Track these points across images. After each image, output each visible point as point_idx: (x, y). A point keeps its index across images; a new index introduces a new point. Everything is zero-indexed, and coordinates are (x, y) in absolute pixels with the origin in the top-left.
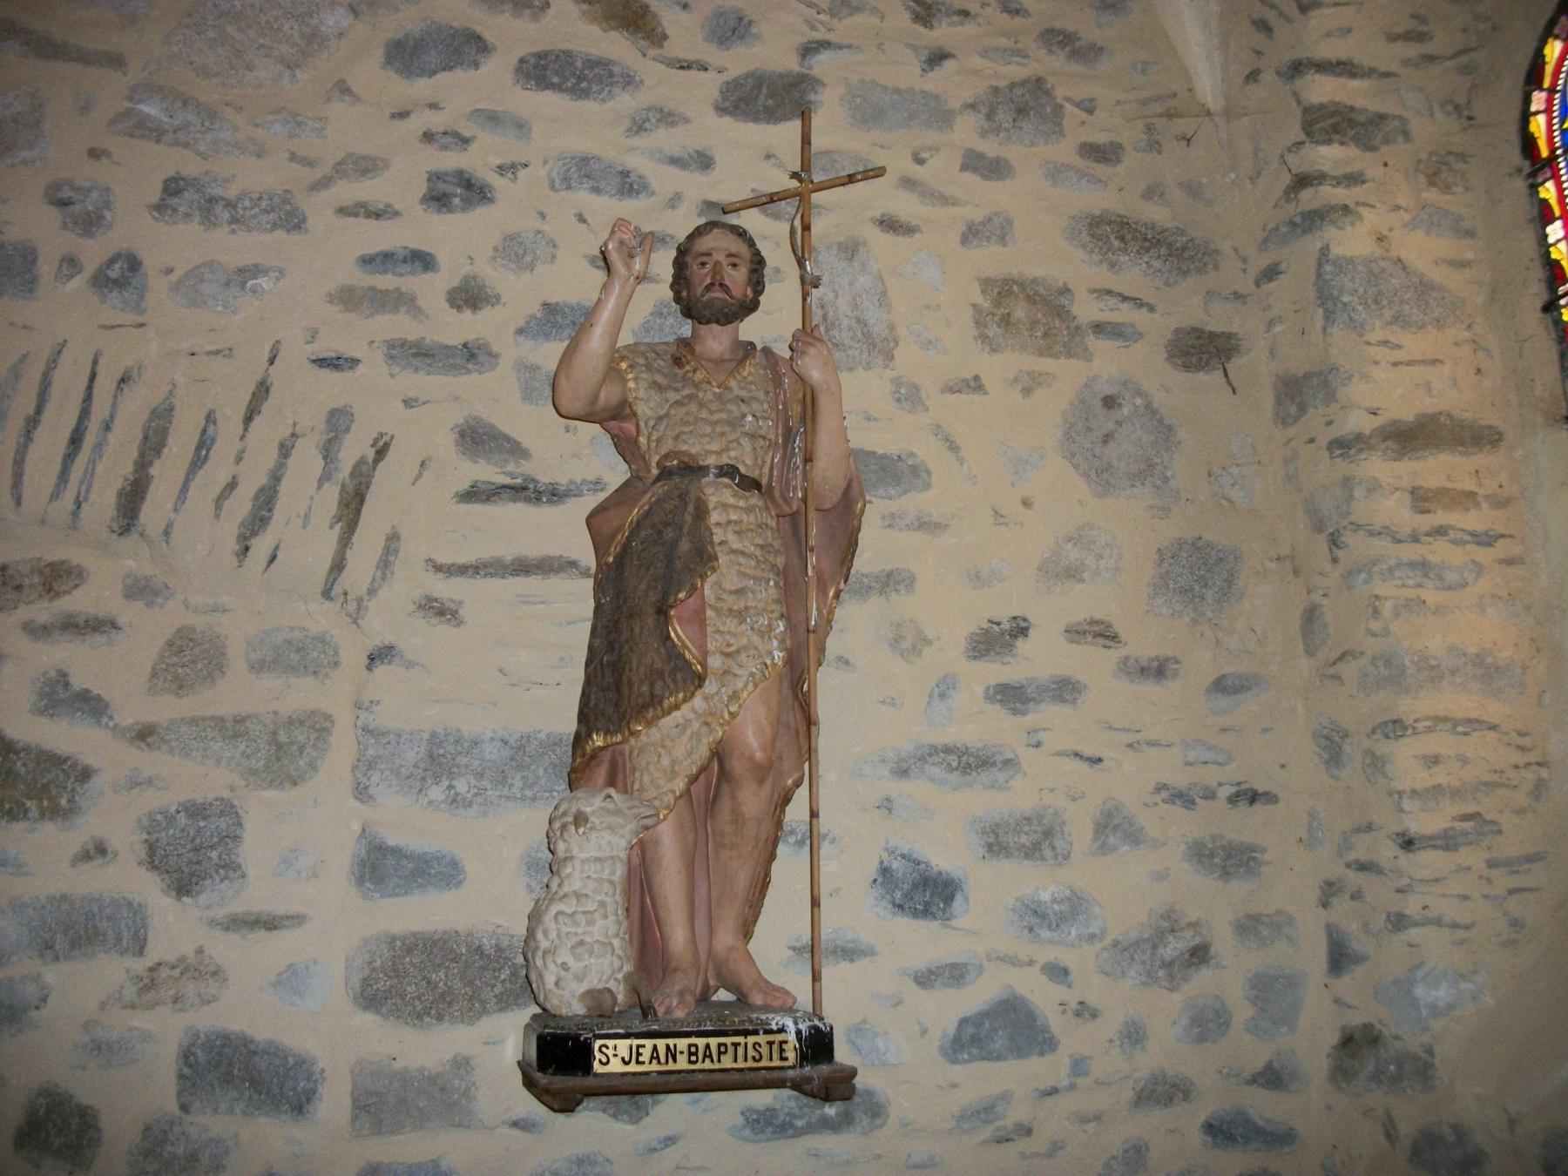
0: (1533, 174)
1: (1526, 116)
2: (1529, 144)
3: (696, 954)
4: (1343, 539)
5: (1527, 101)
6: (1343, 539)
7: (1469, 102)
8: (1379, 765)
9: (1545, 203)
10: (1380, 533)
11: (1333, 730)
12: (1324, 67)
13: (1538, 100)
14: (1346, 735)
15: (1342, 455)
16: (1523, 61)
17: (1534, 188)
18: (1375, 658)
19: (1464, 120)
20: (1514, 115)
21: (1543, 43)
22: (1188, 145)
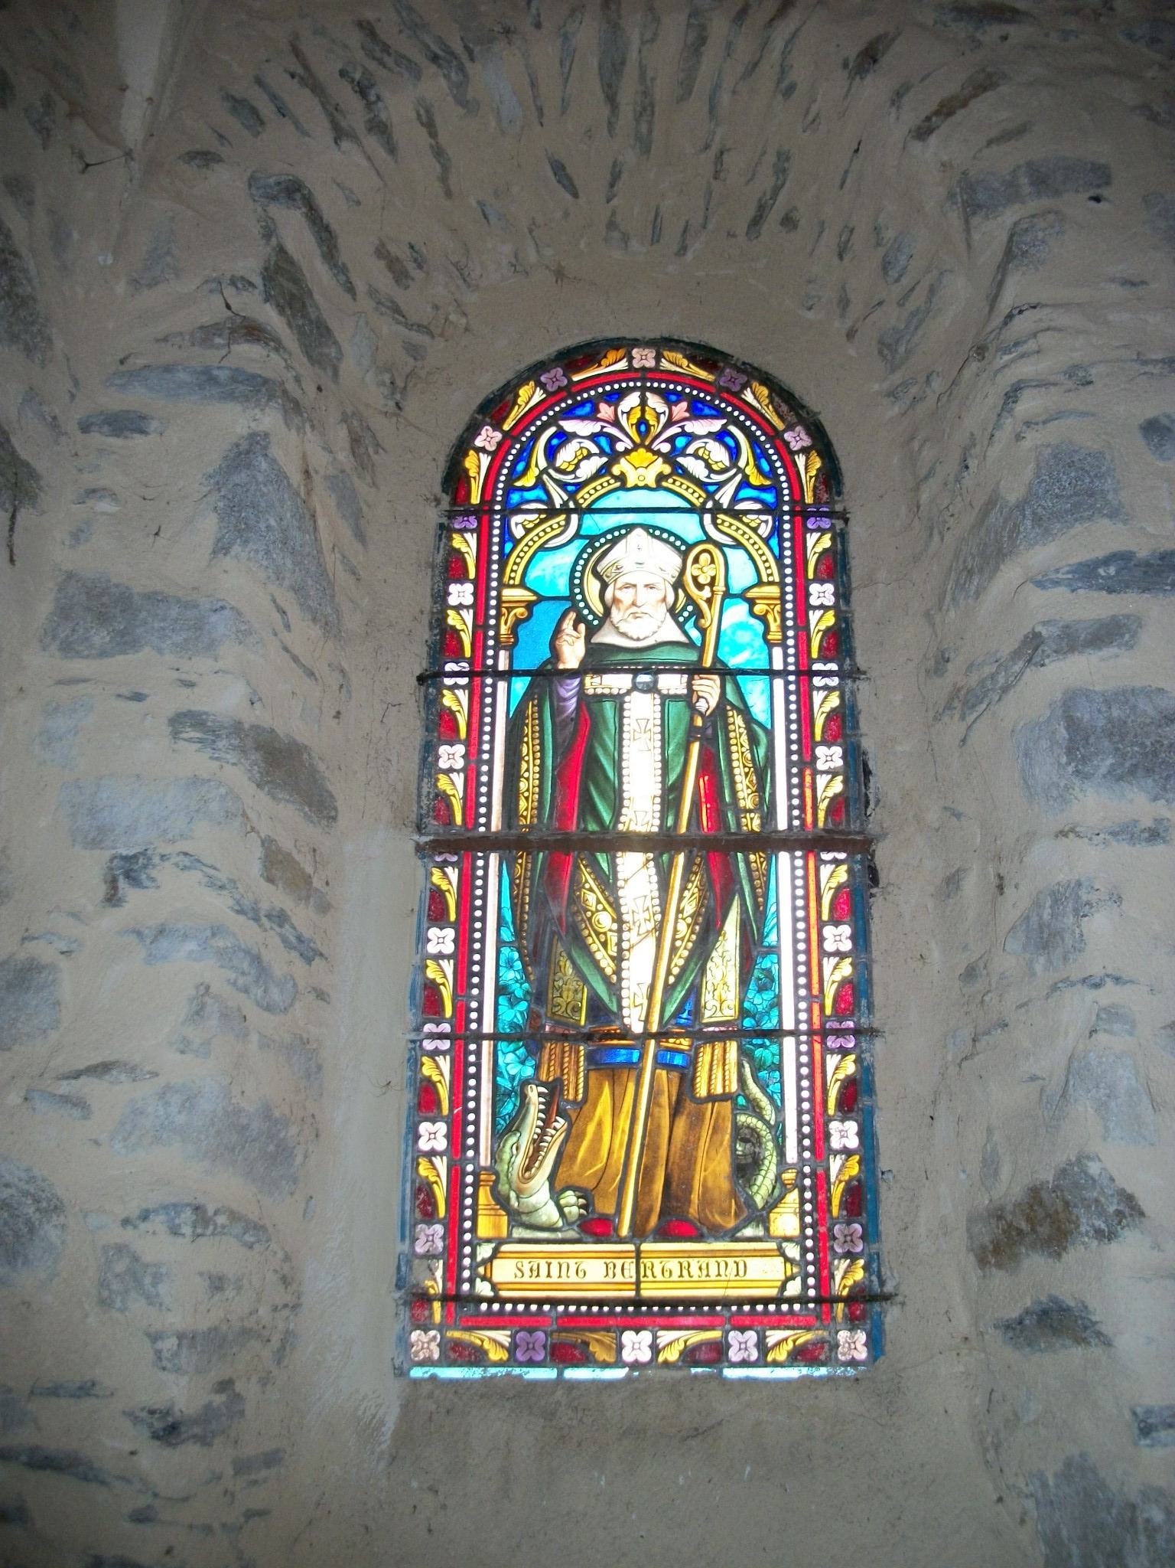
0: (451, 515)
1: (463, 446)
2: (455, 479)
3: (371, 1421)
4: (154, 873)
5: (473, 430)
6: (154, 873)
7: (405, 388)
8: (148, 1280)
9: (458, 557)
10: (221, 887)
11: (26, 1194)
12: (314, 215)
13: (488, 438)
14: (58, 1208)
15: (201, 741)
16: (489, 383)
17: (445, 531)
18: (168, 1088)
19: (391, 403)
20: (453, 435)
21: (521, 380)
22: (83, 172)
